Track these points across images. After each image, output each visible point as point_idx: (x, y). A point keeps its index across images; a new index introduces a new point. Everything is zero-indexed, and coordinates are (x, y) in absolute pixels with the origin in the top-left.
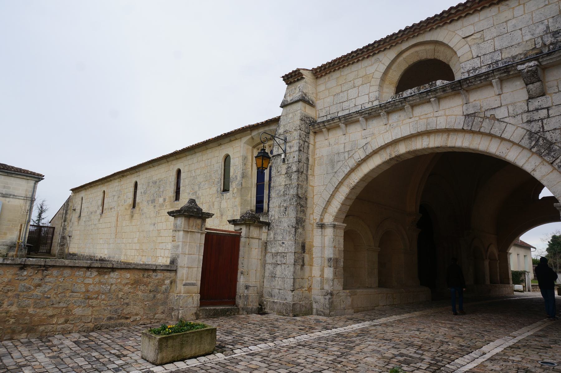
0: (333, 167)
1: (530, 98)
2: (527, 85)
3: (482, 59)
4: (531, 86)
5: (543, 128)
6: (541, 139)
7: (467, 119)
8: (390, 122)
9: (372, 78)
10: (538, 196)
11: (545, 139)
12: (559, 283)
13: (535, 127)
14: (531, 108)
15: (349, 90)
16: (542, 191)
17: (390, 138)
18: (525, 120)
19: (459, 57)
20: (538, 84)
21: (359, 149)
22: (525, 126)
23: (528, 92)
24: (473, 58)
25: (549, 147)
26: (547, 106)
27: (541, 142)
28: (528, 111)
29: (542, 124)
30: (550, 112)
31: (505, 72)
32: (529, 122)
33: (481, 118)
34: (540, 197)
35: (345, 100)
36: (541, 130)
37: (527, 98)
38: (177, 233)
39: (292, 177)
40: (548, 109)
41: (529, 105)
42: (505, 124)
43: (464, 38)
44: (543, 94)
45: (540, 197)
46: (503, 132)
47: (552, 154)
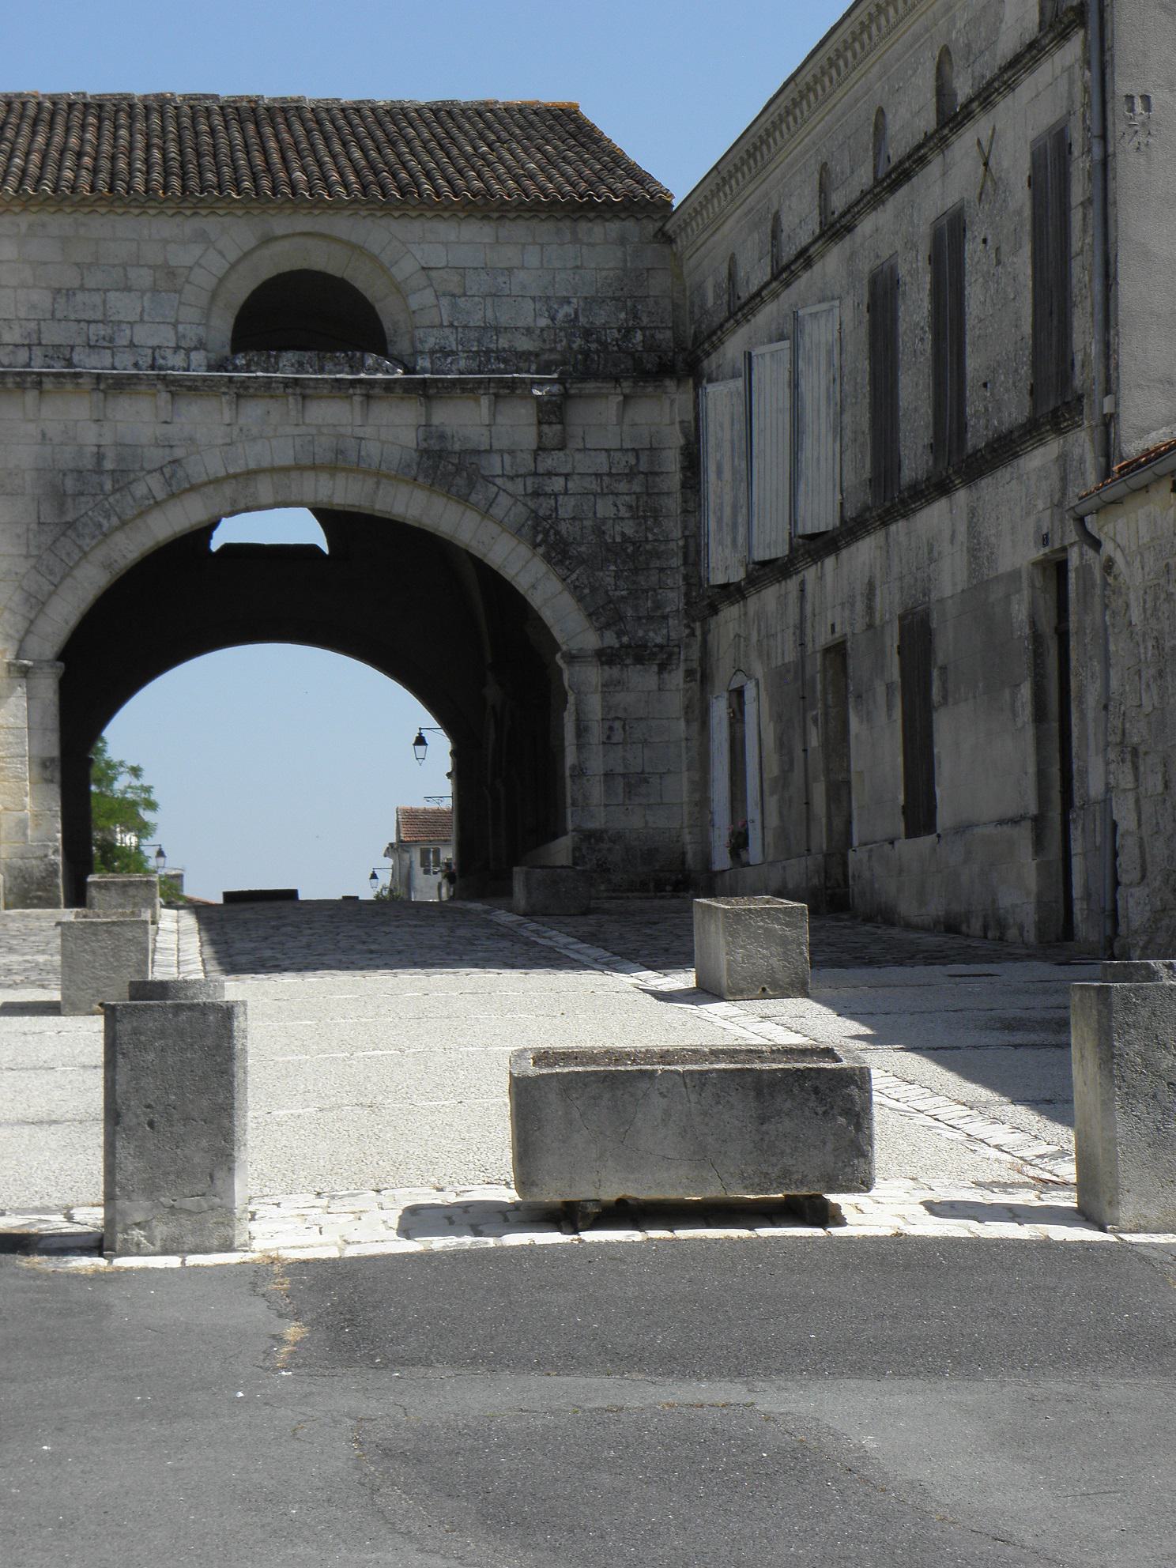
0: (61, 509)
1: (539, 448)
2: (540, 423)
3: (460, 335)
4: (545, 428)
8: (242, 421)
9: (187, 281)
10: (208, 544)
11: (557, 533)
12: (1157, 438)
13: (545, 506)
14: (540, 470)
15: (108, 290)
16: (266, 542)
17: (242, 462)
18: (530, 490)
19: (414, 312)
20: (559, 427)
21: (150, 472)
23: (540, 435)
24: (442, 326)
26: (565, 471)
28: (535, 474)
29: (556, 503)
30: (570, 485)
31: (508, 388)
32: (536, 494)
33: (453, 464)
34: (215, 545)
35: (96, 318)
37: (535, 447)
38: (642, 679)
40: (567, 476)
41: (538, 462)
42: (495, 489)
43: (423, 268)
44: (562, 447)
45: (215, 545)
46: (490, 506)
47: (567, 562)
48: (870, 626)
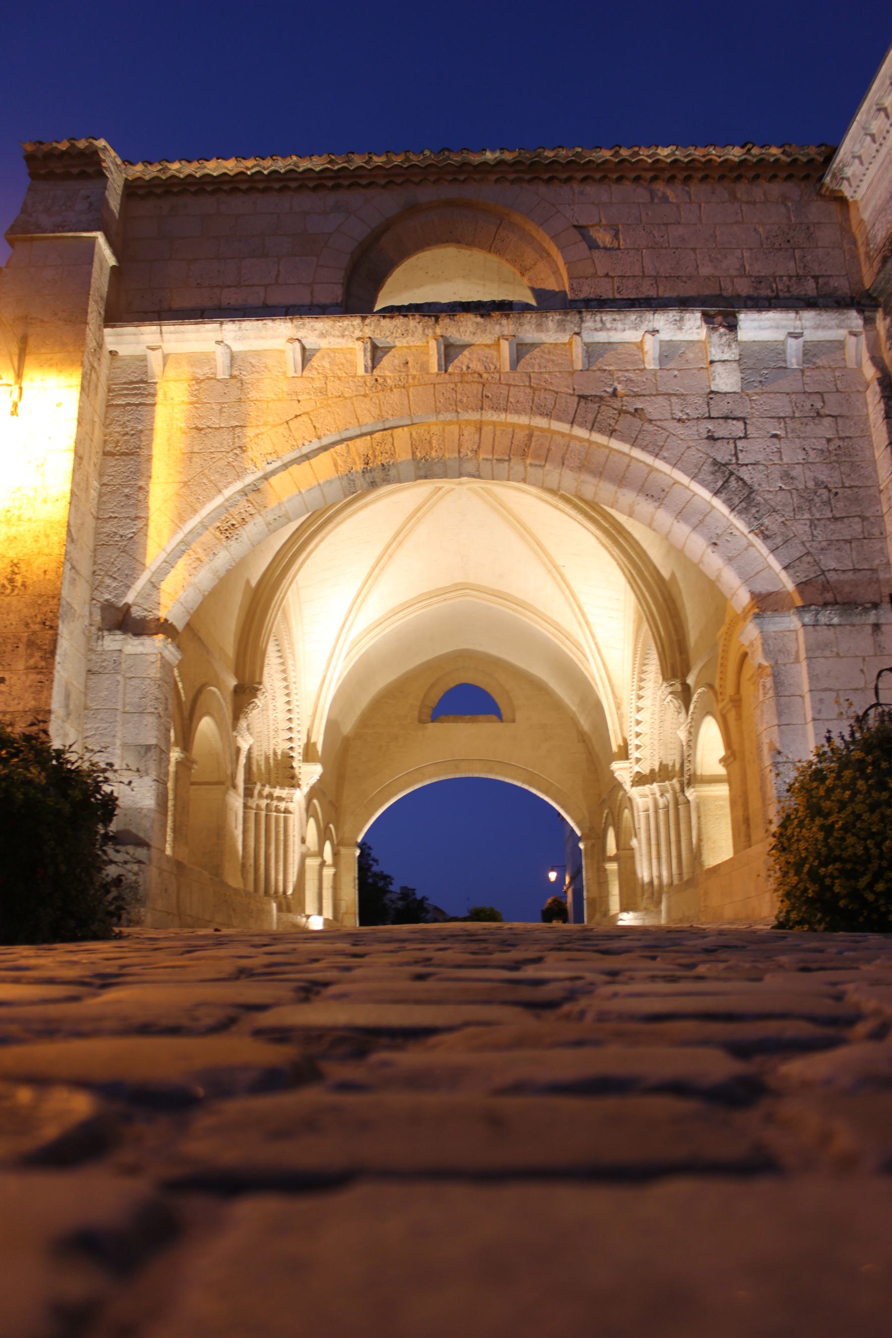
5: (737, 459)
7: (582, 404)
13: (723, 453)
22: (705, 445)
25: (748, 496)
27: (733, 483)
36: (734, 461)
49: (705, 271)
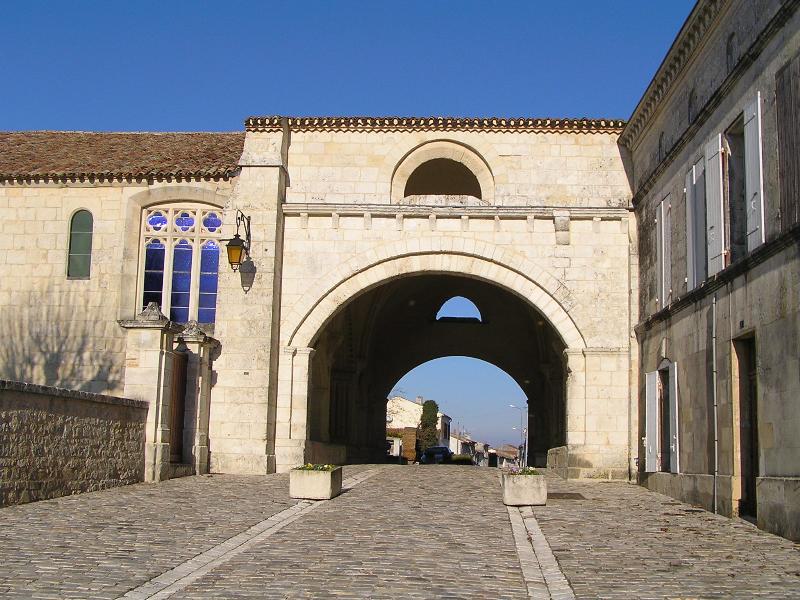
6: (561, 289)
34: (437, 318)
39: (263, 279)
45: (437, 318)
48: (782, 316)
49: (559, 182)
